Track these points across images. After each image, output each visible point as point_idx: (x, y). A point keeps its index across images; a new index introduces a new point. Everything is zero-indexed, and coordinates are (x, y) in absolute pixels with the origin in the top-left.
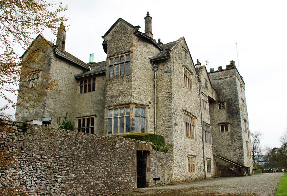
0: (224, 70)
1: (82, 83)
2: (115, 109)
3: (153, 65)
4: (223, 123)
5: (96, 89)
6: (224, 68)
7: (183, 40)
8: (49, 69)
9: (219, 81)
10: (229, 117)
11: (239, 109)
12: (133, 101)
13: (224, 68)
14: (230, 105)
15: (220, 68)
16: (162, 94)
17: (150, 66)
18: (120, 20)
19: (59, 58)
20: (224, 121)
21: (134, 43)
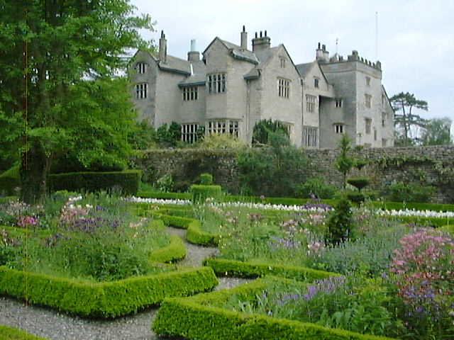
0: (345, 62)
1: (184, 90)
2: (152, 198)
3: (247, 82)
4: (339, 124)
5: (198, 98)
6: (345, 58)
7: (282, 48)
8: (386, 336)
9: (338, 74)
10: (345, 118)
11: (355, 109)
12: (228, 117)
13: (345, 58)
14: (346, 104)
15: (341, 58)
16: (253, 109)
17: (244, 83)
18: (216, 39)
19: (163, 70)
20: (340, 122)
21: (229, 63)
